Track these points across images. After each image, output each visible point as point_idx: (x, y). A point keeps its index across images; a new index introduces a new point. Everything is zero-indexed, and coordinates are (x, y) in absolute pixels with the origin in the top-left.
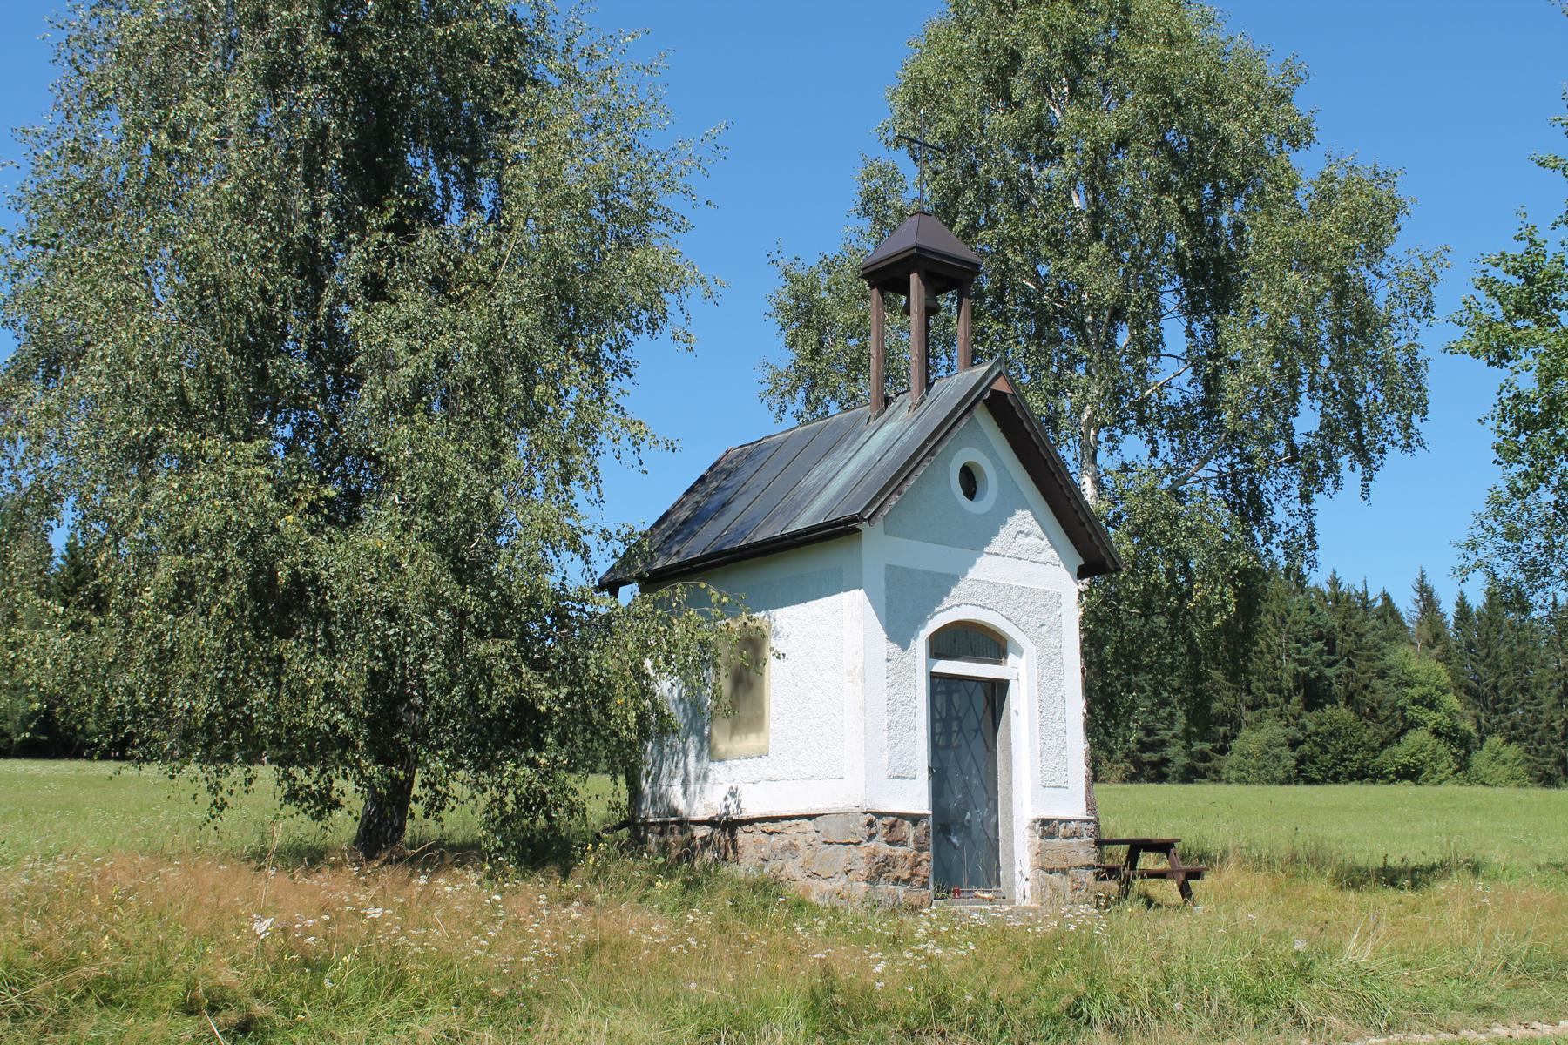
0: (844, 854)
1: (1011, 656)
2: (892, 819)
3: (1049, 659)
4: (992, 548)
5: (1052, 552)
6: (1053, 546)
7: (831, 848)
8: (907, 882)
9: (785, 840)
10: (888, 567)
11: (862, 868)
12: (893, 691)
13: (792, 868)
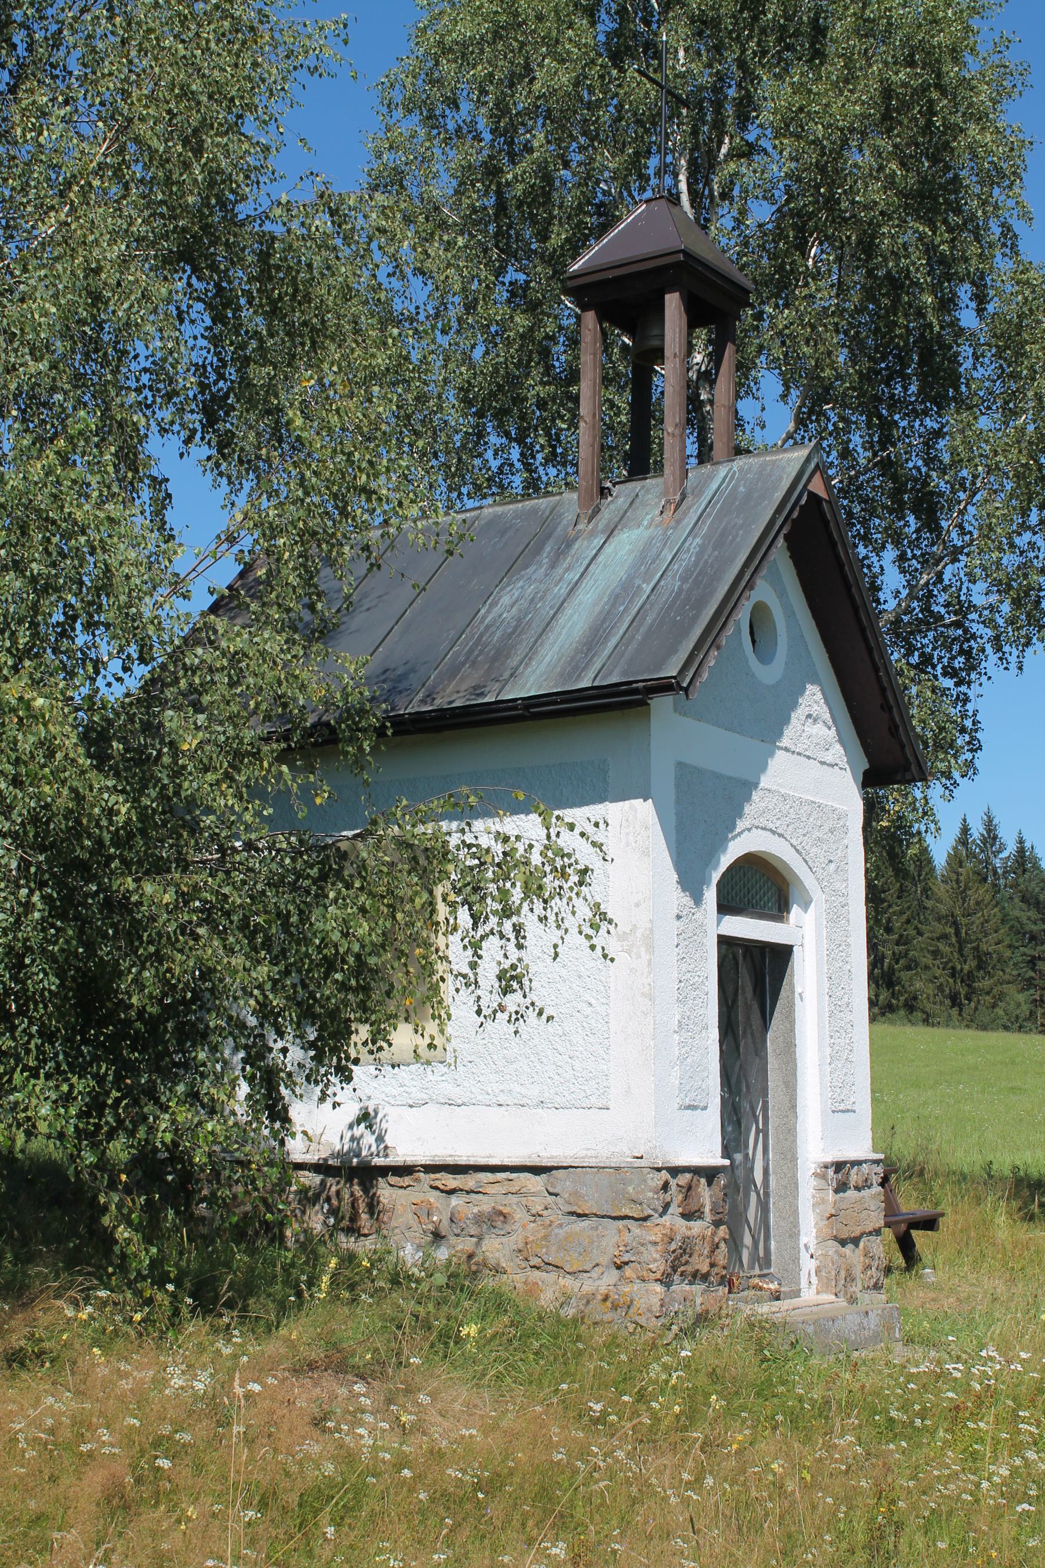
0: (611, 1238)
1: (795, 911)
2: (688, 1176)
3: (836, 917)
4: (785, 742)
5: (838, 749)
6: (841, 741)
7: (585, 1223)
8: (705, 1277)
9: (485, 1204)
10: (680, 765)
11: (656, 1261)
12: (684, 967)
13: (495, 1248)
